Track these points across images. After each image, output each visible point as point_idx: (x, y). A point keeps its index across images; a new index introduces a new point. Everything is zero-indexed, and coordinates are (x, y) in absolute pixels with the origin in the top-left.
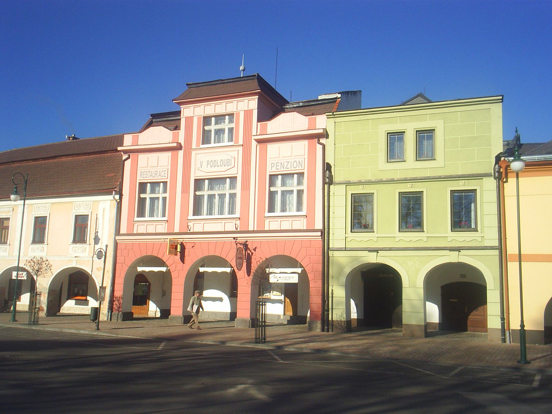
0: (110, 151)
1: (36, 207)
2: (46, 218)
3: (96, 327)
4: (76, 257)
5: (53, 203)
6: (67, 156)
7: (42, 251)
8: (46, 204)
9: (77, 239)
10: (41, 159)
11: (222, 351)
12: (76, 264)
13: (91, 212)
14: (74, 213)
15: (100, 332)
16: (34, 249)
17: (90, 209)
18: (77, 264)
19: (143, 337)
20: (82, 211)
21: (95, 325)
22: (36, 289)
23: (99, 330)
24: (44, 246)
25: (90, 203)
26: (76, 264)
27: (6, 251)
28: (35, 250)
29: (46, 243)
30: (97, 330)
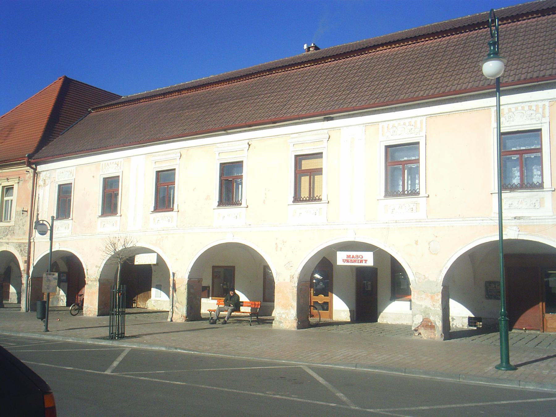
0: (152, 98)
1: (104, 165)
2: (321, 155)
3: (44, 328)
4: (515, 218)
5: (431, 115)
6: (391, 46)
7: (67, 229)
8: (414, 119)
9: (224, 201)
10: (330, 57)
11: (392, 375)
12: (518, 233)
13: (75, 179)
14: (101, 176)
15: (50, 335)
16: (57, 227)
17: (544, 116)
18: (520, 233)
19: (425, 373)
20: (64, 180)
21: (44, 324)
22: (171, 284)
23: (48, 331)
24: (420, 201)
25: (540, 104)
26: (518, 233)
27: (68, 228)
28: (58, 228)
29: (119, 214)
30: (46, 331)
